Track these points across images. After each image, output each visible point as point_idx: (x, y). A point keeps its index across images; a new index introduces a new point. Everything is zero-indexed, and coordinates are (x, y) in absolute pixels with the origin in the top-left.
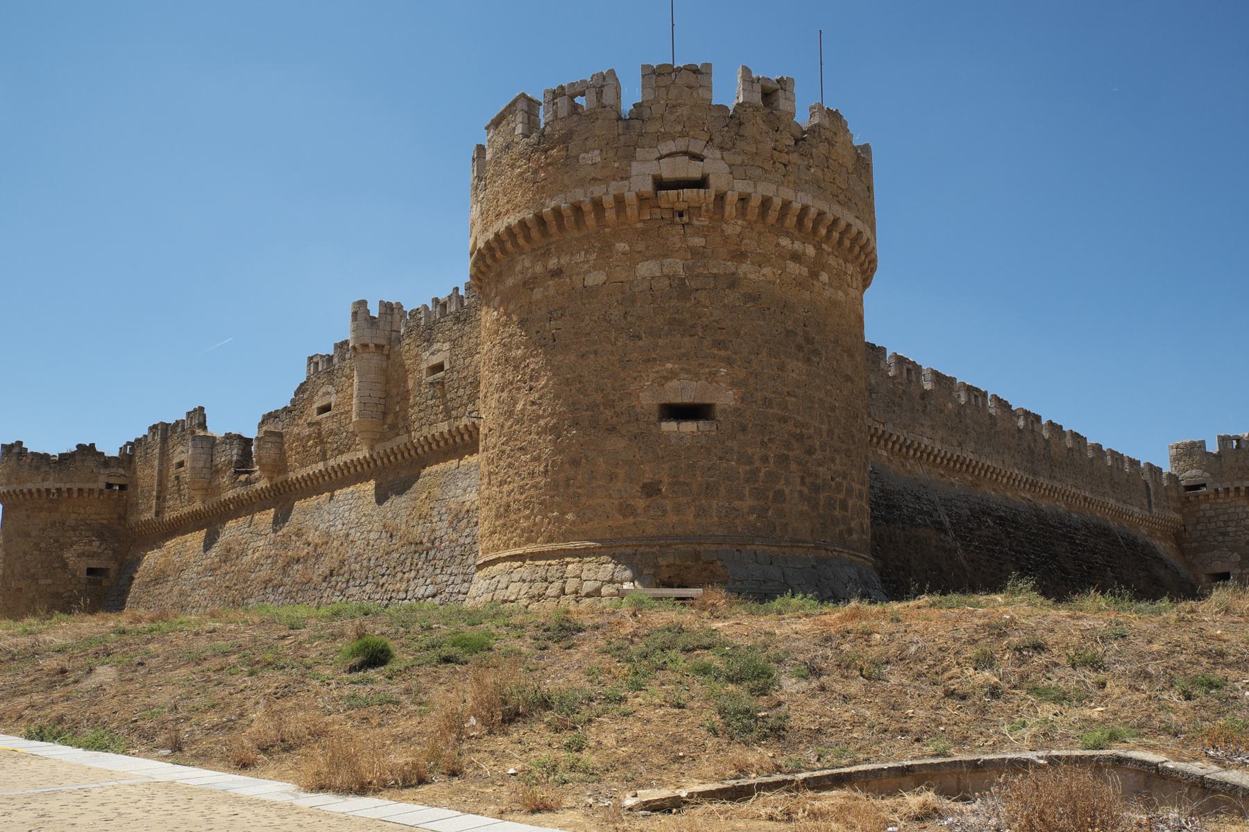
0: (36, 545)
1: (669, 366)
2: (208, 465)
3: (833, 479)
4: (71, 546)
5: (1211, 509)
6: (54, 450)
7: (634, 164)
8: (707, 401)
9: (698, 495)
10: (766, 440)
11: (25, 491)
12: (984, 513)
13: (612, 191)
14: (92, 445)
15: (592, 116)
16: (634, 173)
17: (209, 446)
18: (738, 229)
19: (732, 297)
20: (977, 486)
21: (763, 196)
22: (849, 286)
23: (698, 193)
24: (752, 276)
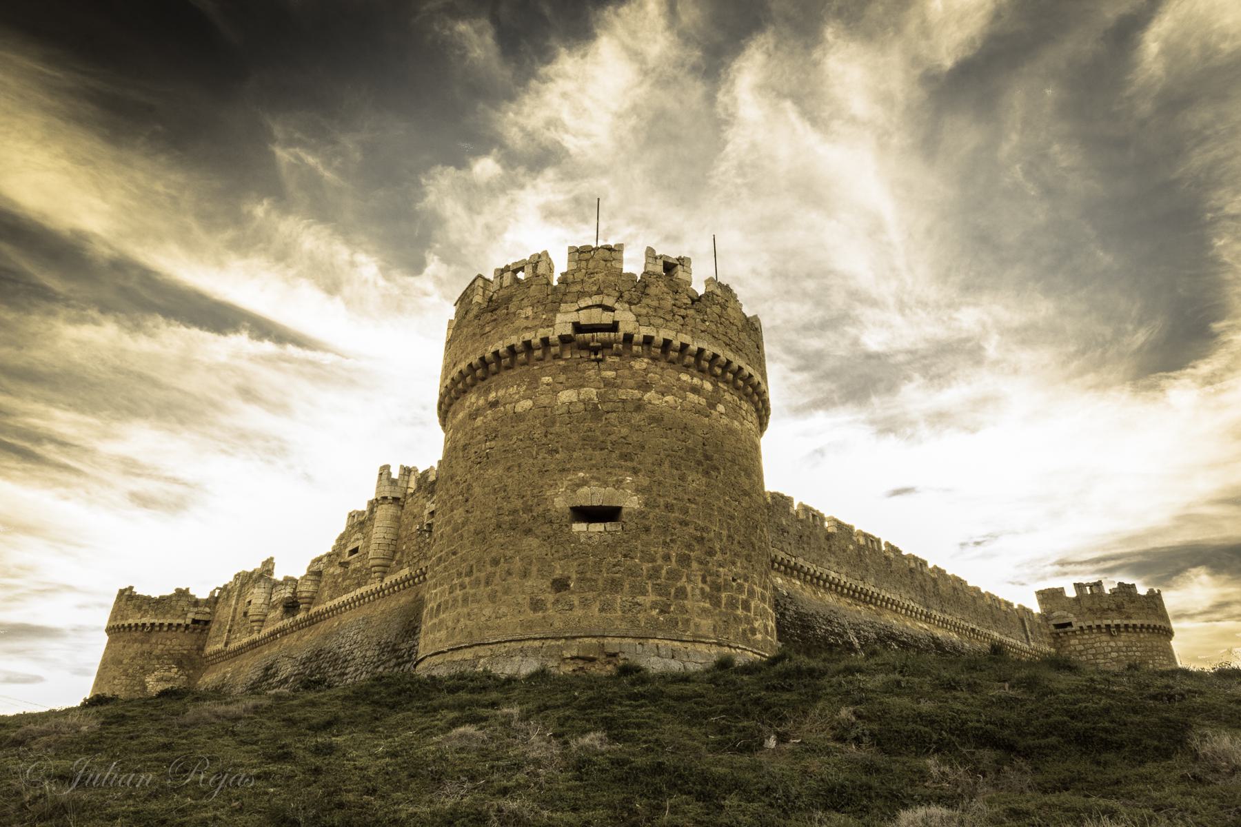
0: (125, 670)
1: (581, 474)
2: (267, 602)
3: (734, 580)
4: (153, 672)
5: (1080, 644)
6: (155, 594)
7: (558, 315)
8: (615, 504)
9: (603, 590)
10: (668, 540)
11: (126, 625)
12: (889, 638)
13: (539, 336)
14: (187, 589)
15: (528, 284)
16: (558, 321)
17: (270, 586)
18: (644, 366)
19: (637, 418)
20: (881, 615)
21: (664, 339)
22: (744, 418)
23: (609, 336)
24: (657, 402)
